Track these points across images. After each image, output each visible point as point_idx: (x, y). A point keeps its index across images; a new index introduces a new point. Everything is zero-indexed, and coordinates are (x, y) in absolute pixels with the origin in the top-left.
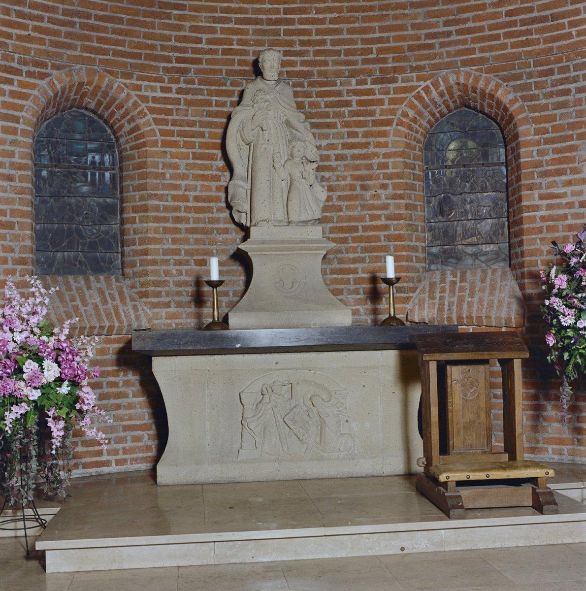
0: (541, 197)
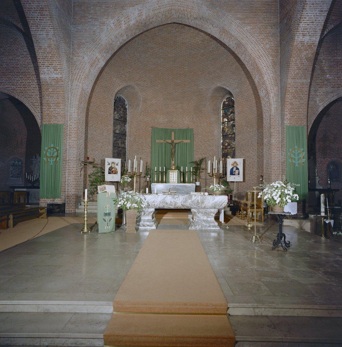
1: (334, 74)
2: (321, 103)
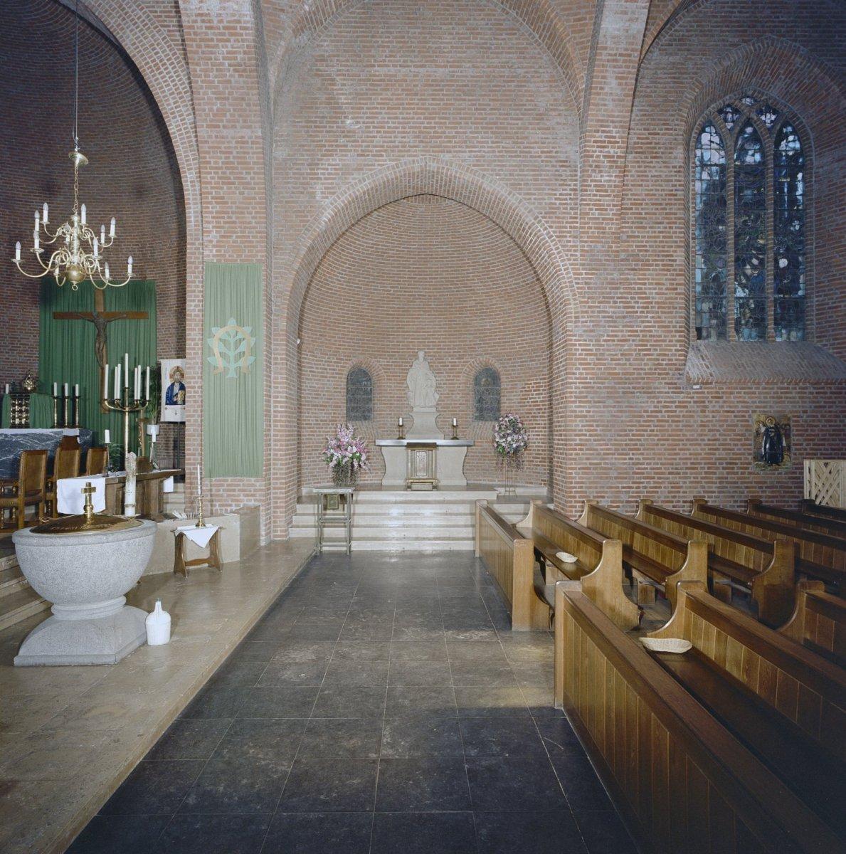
1: (367, 118)
2: (327, 198)
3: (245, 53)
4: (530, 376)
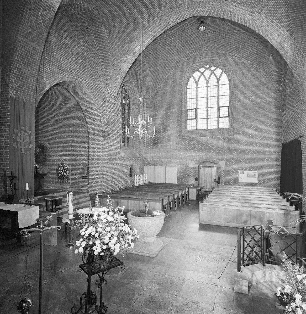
0: (52, 158)
2: (47, 80)
3: (49, 18)
4: (63, 150)
